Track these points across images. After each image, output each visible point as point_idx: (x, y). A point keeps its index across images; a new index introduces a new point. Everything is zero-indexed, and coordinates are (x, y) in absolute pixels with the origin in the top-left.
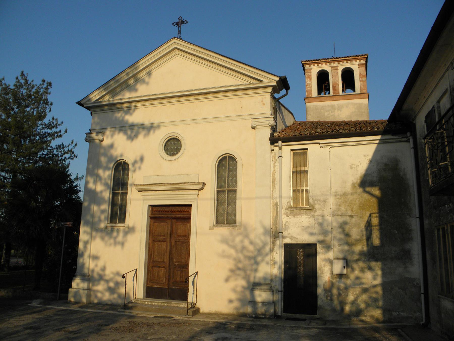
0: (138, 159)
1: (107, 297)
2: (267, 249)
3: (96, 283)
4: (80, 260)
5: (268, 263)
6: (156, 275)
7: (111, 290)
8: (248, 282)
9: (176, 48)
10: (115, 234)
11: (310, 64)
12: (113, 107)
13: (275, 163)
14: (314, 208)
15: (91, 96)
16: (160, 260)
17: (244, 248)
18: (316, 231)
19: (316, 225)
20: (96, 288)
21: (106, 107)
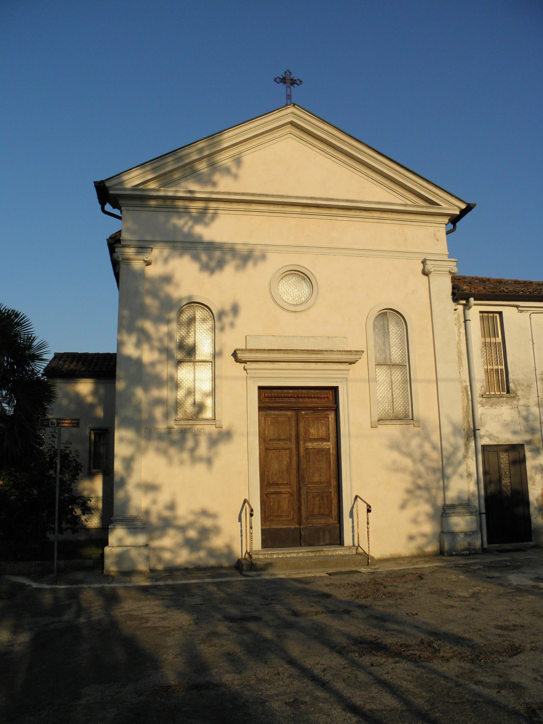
0: (228, 307)
1: (184, 557)
2: (460, 454)
3: (157, 534)
5: (461, 476)
6: (276, 507)
7: (192, 545)
8: (434, 506)
9: (292, 124)
10: (190, 443)
12: (169, 204)
13: (459, 329)
14: (517, 396)
15: (126, 177)
16: (280, 482)
17: (424, 456)
18: (518, 428)
19: (521, 420)
20: (156, 543)
21: (153, 203)
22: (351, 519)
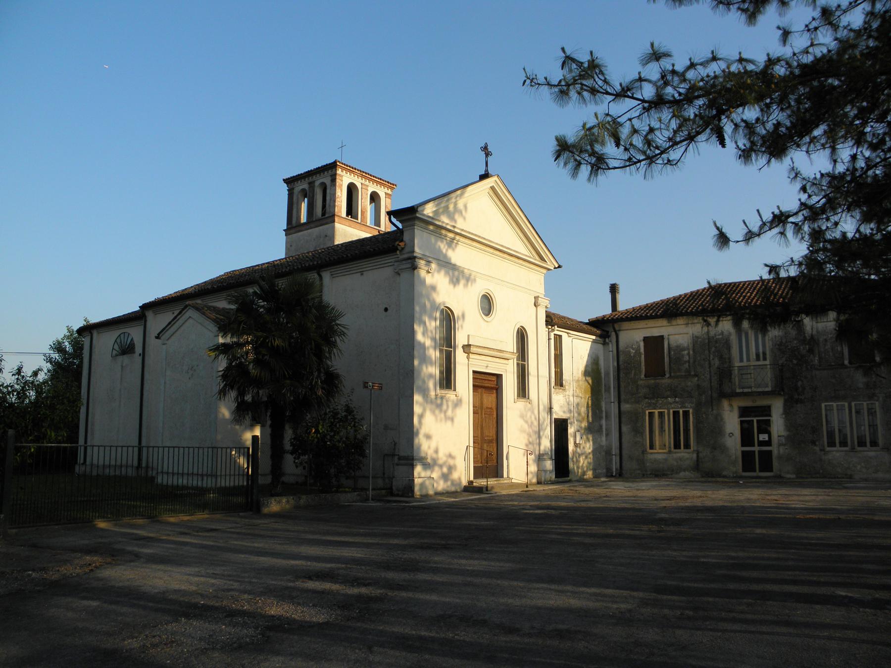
4: (416, 441)
11: (343, 169)
21: (431, 227)
22: (718, 225)
